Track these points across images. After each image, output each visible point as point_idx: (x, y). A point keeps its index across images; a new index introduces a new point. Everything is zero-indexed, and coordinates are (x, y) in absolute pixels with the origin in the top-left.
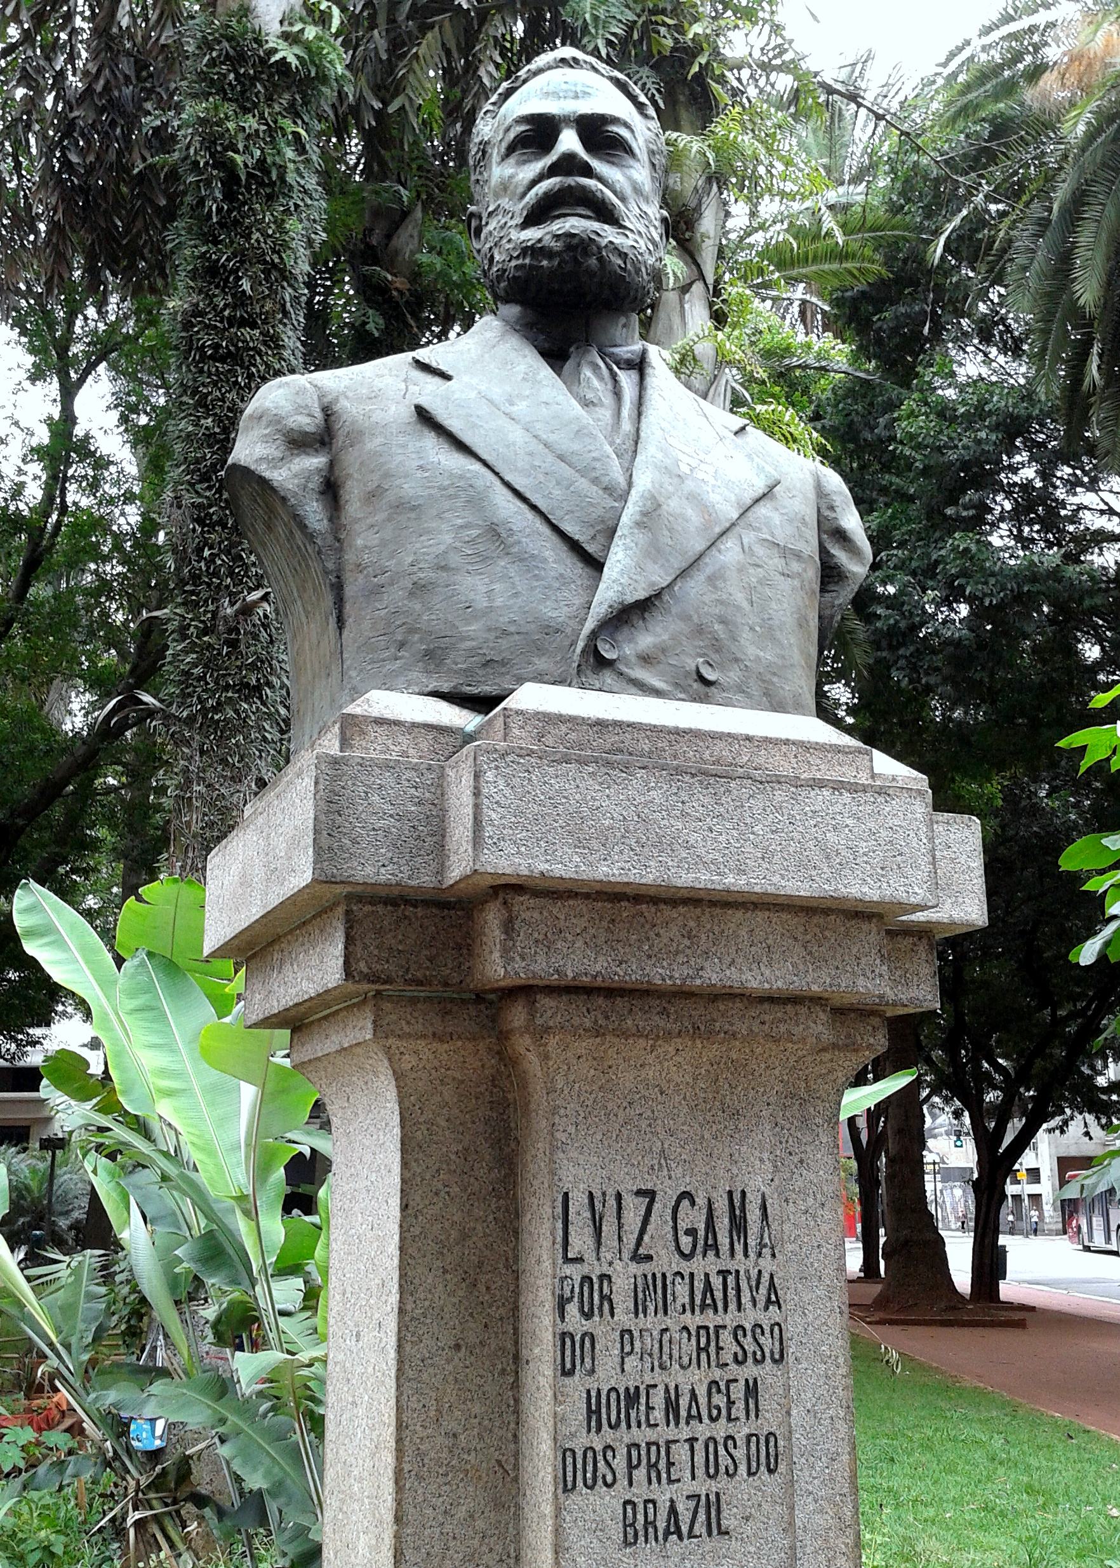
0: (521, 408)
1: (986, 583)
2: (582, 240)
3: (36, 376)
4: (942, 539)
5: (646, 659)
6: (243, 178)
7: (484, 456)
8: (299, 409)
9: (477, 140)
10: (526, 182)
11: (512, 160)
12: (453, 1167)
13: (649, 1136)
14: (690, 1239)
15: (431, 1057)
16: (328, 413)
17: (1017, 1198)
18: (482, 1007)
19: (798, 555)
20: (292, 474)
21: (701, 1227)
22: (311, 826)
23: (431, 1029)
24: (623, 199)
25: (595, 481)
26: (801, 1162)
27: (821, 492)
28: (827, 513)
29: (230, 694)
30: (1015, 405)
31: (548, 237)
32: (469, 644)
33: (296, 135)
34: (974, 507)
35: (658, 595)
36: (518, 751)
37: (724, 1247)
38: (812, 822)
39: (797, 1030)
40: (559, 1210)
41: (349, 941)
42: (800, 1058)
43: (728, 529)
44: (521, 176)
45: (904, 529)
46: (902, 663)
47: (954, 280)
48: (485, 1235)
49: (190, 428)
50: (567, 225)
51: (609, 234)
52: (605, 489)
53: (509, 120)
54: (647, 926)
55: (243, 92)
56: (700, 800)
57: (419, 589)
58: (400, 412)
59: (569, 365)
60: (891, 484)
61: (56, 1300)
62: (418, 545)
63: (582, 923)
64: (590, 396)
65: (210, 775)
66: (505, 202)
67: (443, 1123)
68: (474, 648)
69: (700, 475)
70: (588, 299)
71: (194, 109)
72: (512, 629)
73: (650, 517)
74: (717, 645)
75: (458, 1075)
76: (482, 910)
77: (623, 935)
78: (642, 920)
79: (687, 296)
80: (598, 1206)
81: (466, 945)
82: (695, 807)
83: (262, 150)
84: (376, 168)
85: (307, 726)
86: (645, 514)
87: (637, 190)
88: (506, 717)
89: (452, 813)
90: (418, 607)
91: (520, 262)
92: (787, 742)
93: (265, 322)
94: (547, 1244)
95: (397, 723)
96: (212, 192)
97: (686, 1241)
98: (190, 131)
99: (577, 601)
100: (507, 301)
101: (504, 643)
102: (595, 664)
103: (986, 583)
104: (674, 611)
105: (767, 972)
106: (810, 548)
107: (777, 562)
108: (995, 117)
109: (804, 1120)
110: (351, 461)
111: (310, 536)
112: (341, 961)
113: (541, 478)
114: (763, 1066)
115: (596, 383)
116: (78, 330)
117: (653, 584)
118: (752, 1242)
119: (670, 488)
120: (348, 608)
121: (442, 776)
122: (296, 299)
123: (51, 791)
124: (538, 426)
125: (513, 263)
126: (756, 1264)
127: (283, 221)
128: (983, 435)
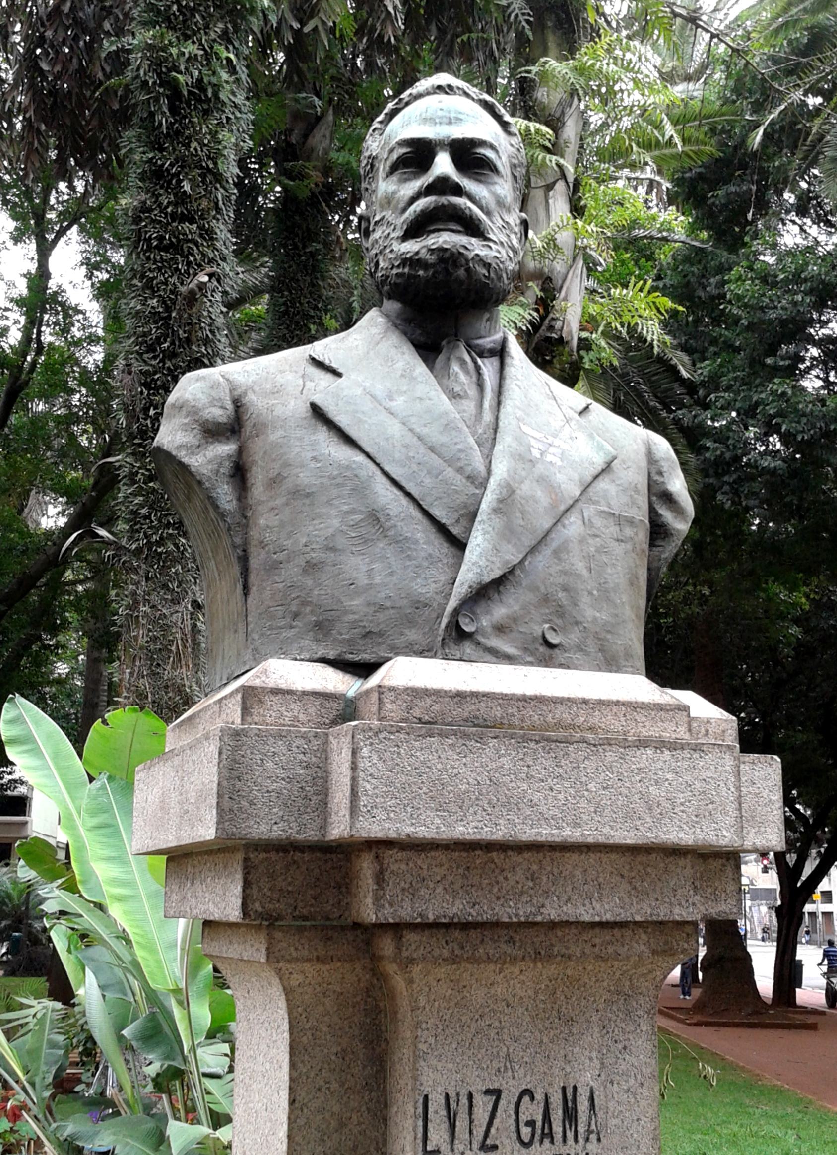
0: (399, 403)
1: (799, 422)
2: (452, 254)
3: (17, 238)
4: (761, 384)
5: (500, 629)
6: (186, 93)
7: (368, 450)
8: (213, 402)
9: (367, 154)
10: (406, 199)
11: (395, 178)
12: (333, 1066)
13: (496, 1043)
14: (529, 1129)
15: (316, 975)
16: (238, 404)
17: (813, 915)
18: (359, 932)
19: (631, 522)
20: (207, 459)
21: (539, 1118)
22: (215, 790)
23: (315, 954)
24: (488, 213)
25: (460, 470)
26: (625, 1048)
27: (651, 458)
28: (656, 478)
29: (171, 531)
30: (826, 274)
31: (424, 251)
32: (351, 617)
33: (229, 60)
34: (789, 358)
35: (511, 571)
36: (389, 729)
37: (558, 1136)
38: (638, 778)
39: (623, 950)
40: (420, 1110)
41: (247, 885)
42: (625, 972)
43: (571, 506)
44: (402, 193)
45: (731, 375)
46: (726, 488)
47: (777, 164)
48: (359, 1124)
49: (139, 307)
50: (441, 240)
51: (475, 247)
52: (468, 477)
53: (394, 142)
54: (497, 871)
55: (184, 21)
56: (543, 763)
57: (311, 567)
58: (297, 408)
59: (441, 358)
60: (721, 335)
61: (24, 1043)
62: (311, 528)
63: (442, 871)
64: (457, 389)
65: (154, 598)
66: (389, 215)
67: (325, 1029)
68: (355, 621)
69: (549, 458)
70: (458, 301)
71: (146, 36)
72: (388, 604)
73: (507, 502)
74: (560, 612)
75: (339, 990)
76: (359, 857)
77: (476, 880)
78: (493, 866)
79: (551, 193)
80: (453, 1105)
81: (345, 885)
82: (539, 771)
83: (200, 73)
84: (296, 79)
85: (218, 666)
86: (501, 501)
87: (500, 203)
88: (380, 693)
89: (334, 777)
90: (310, 583)
91: (400, 271)
92: (617, 703)
93: (202, 218)
94: (410, 1137)
95: (290, 692)
96: (160, 108)
97: (526, 1131)
98: (140, 55)
99: (443, 578)
100: (389, 298)
101: (381, 617)
102: (456, 638)
103: (799, 422)
104: (524, 583)
105: (598, 906)
106: (641, 515)
107: (613, 530)
108: (812, 27)
109: (628, 1013)
110: (257, 451)
111: (222, 515)
112: (239, 901)
113: (415, 467)
114: (594, 979)
115: (463, 377)
116: (52, 201)
117: (507, 562)
118: (581, 1129)
119: (524, 473)
120: (252, 578)
121: (326, 742)
122: (227, 199)
123: (27, 583)
124: (413, 420)
125: (395, 271)
126: (585, 1148)
127: (217, 132)
128: (799, 298)
